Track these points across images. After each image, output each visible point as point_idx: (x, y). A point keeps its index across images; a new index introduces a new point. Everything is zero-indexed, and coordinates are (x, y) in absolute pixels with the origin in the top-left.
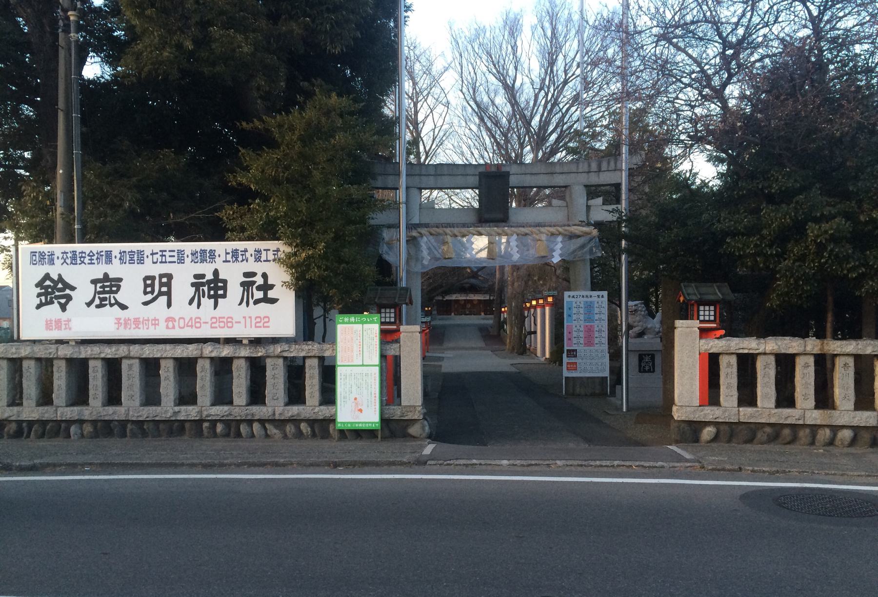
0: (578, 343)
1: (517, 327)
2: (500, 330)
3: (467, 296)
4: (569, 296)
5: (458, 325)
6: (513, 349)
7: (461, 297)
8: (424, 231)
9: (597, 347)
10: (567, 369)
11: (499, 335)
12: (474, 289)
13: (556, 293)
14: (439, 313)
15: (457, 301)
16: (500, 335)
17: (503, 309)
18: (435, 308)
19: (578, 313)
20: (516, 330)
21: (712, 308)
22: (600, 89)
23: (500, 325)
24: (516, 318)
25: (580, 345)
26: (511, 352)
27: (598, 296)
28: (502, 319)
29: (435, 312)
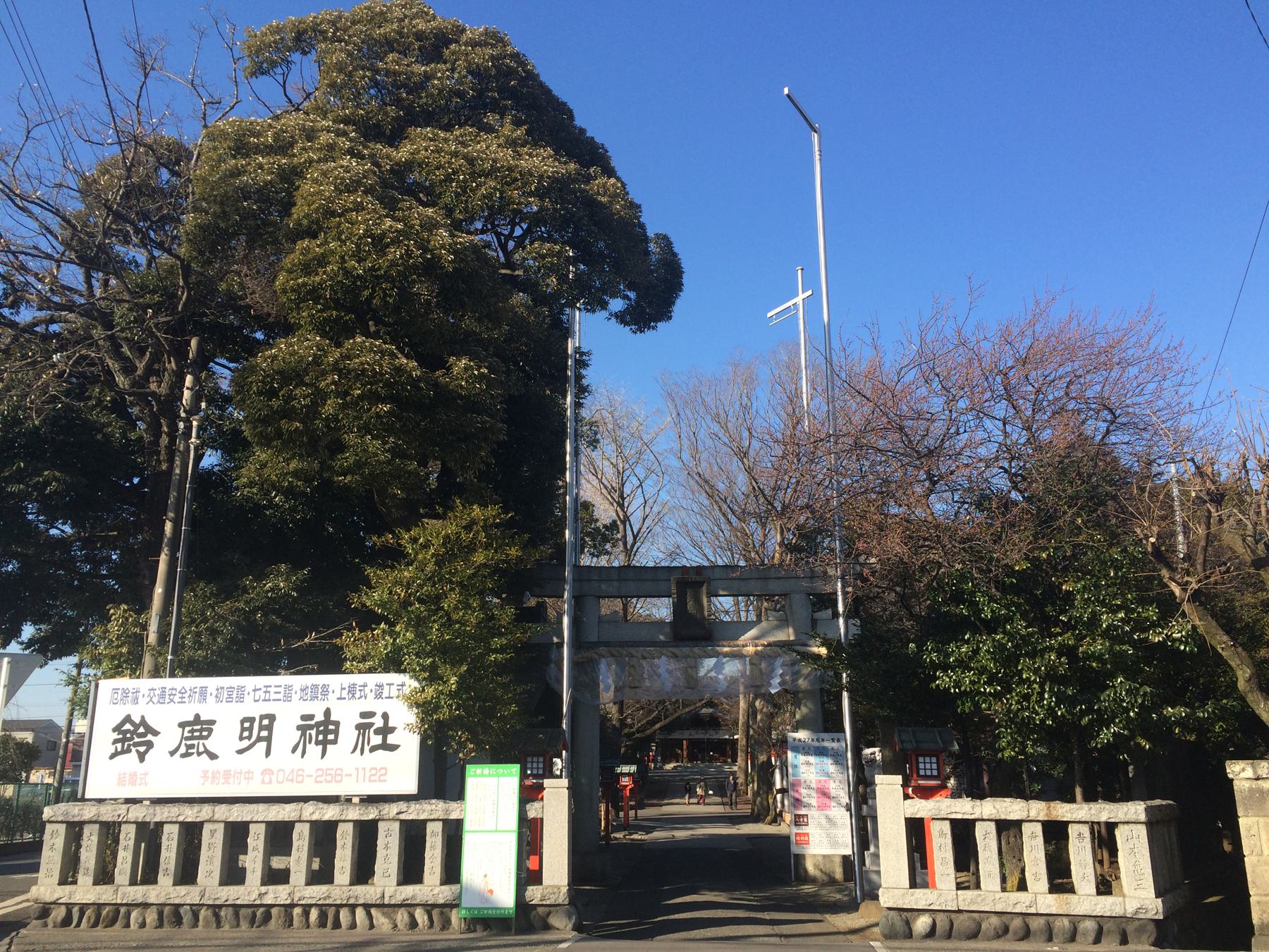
8: (602, 650)
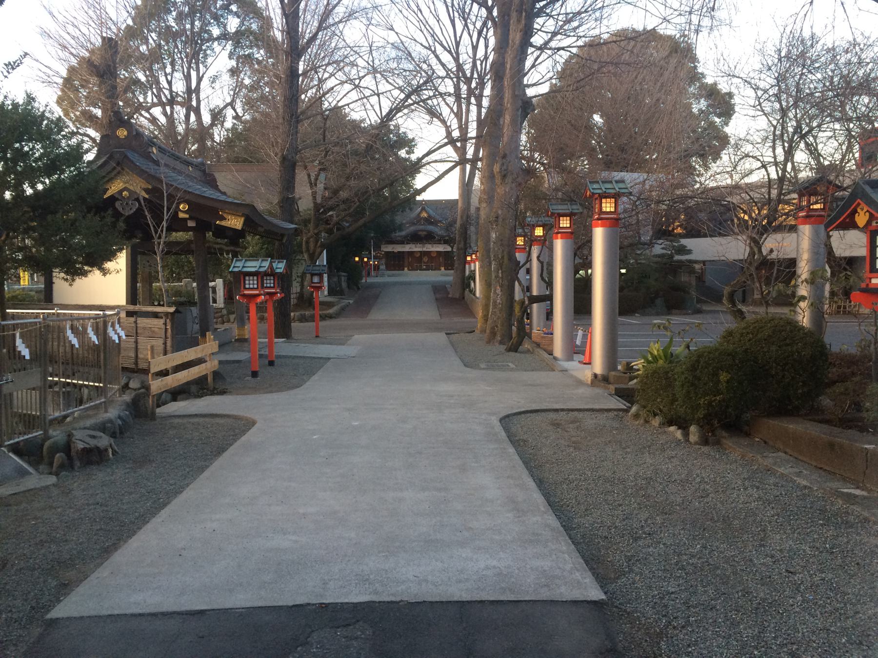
1: (501, 286)
2: (464, 290)
3: (424, 247)
5: (410, 283)
6: (493, 334)
7: (416, 248)
11: (463, 297)
12: (429, 238)
13: (577, 208)
14: (388, 268)
15: (411, 253)
16: (464, 298)
17: (469, 258)
18: (383, 261)
20: (499, 291)
21: (255, 278)
22: (425, 83)
23: (466, 282)
24: (500, 266)
26: (489, 342)
28: (467, 273)
29: (383, 267)
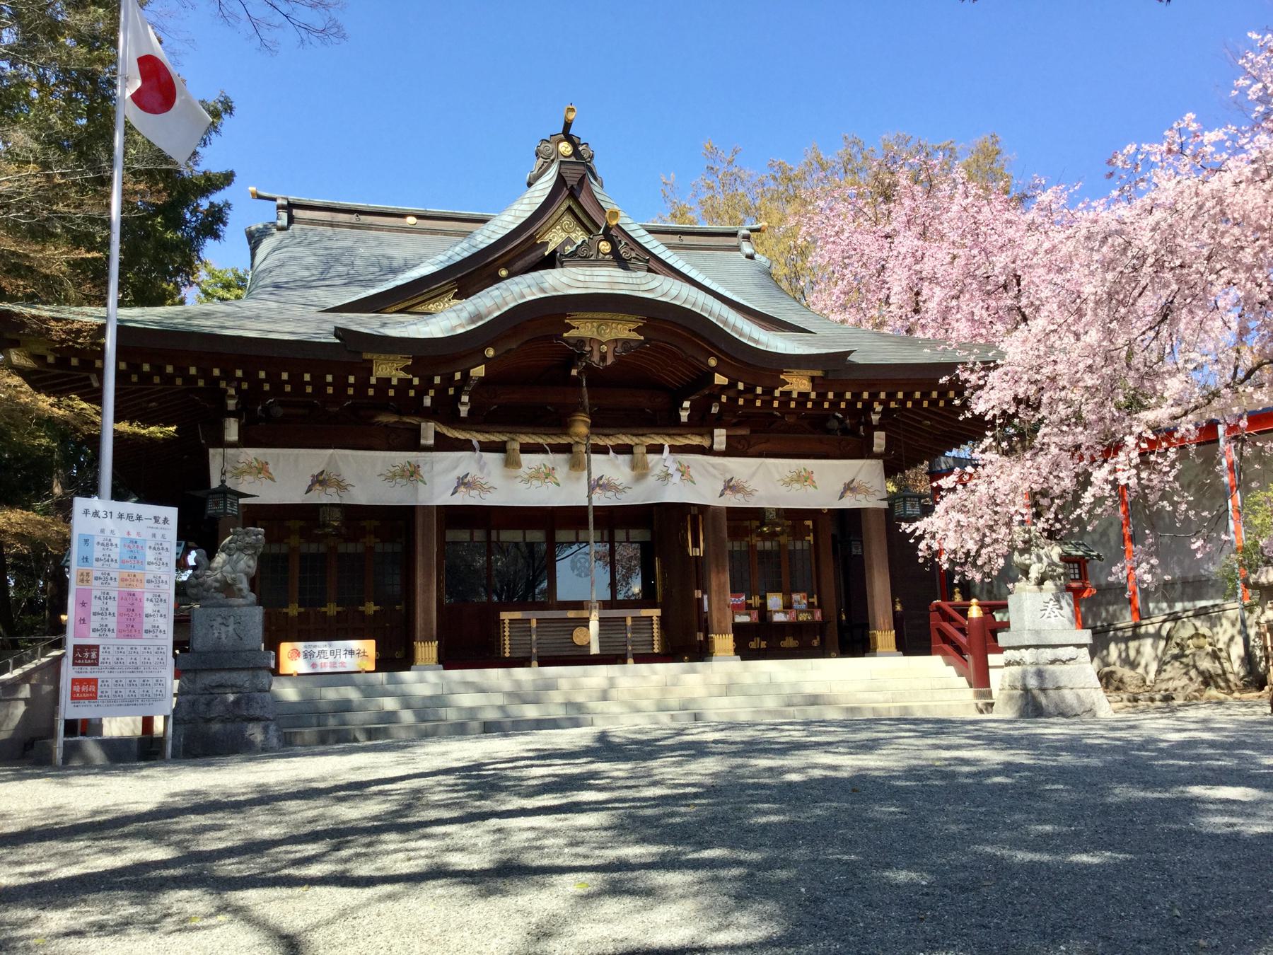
0: (103, 630)
4: (86, 512)
9: (146, 640)
10: (72, 698)
19: (103, 613)
21: (1076, 566)
25: (110, 634)
27: (156, 519)
